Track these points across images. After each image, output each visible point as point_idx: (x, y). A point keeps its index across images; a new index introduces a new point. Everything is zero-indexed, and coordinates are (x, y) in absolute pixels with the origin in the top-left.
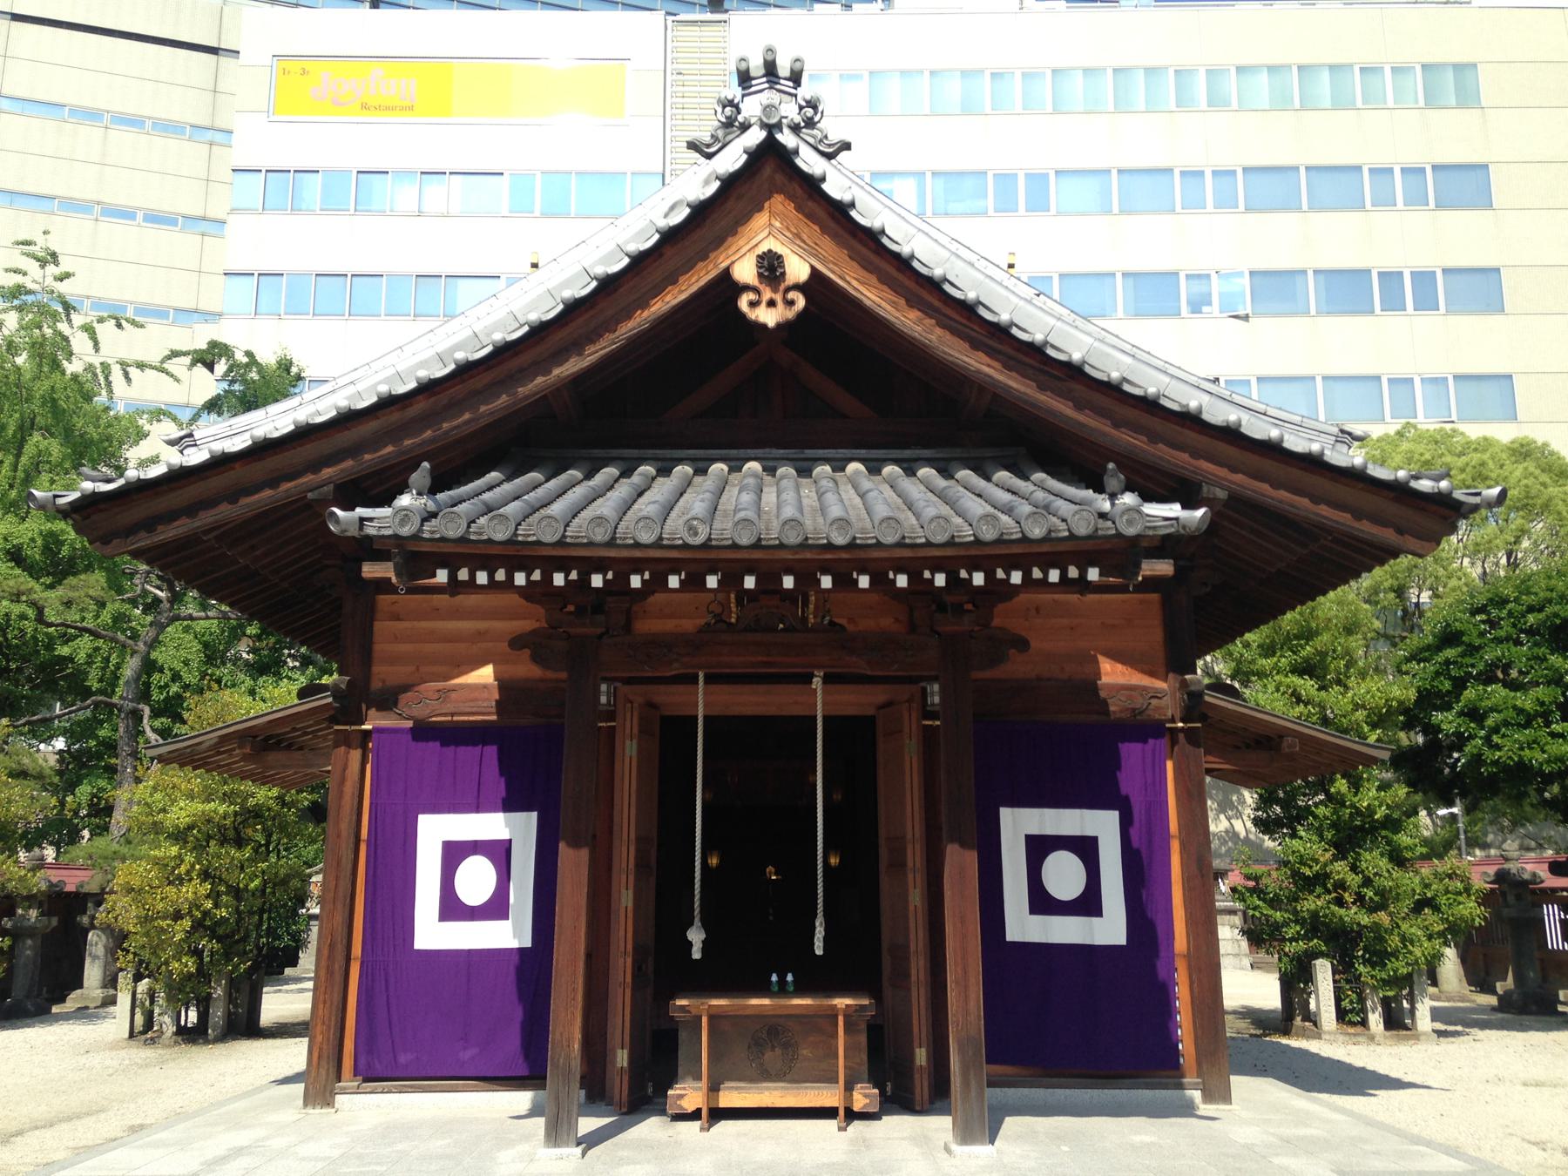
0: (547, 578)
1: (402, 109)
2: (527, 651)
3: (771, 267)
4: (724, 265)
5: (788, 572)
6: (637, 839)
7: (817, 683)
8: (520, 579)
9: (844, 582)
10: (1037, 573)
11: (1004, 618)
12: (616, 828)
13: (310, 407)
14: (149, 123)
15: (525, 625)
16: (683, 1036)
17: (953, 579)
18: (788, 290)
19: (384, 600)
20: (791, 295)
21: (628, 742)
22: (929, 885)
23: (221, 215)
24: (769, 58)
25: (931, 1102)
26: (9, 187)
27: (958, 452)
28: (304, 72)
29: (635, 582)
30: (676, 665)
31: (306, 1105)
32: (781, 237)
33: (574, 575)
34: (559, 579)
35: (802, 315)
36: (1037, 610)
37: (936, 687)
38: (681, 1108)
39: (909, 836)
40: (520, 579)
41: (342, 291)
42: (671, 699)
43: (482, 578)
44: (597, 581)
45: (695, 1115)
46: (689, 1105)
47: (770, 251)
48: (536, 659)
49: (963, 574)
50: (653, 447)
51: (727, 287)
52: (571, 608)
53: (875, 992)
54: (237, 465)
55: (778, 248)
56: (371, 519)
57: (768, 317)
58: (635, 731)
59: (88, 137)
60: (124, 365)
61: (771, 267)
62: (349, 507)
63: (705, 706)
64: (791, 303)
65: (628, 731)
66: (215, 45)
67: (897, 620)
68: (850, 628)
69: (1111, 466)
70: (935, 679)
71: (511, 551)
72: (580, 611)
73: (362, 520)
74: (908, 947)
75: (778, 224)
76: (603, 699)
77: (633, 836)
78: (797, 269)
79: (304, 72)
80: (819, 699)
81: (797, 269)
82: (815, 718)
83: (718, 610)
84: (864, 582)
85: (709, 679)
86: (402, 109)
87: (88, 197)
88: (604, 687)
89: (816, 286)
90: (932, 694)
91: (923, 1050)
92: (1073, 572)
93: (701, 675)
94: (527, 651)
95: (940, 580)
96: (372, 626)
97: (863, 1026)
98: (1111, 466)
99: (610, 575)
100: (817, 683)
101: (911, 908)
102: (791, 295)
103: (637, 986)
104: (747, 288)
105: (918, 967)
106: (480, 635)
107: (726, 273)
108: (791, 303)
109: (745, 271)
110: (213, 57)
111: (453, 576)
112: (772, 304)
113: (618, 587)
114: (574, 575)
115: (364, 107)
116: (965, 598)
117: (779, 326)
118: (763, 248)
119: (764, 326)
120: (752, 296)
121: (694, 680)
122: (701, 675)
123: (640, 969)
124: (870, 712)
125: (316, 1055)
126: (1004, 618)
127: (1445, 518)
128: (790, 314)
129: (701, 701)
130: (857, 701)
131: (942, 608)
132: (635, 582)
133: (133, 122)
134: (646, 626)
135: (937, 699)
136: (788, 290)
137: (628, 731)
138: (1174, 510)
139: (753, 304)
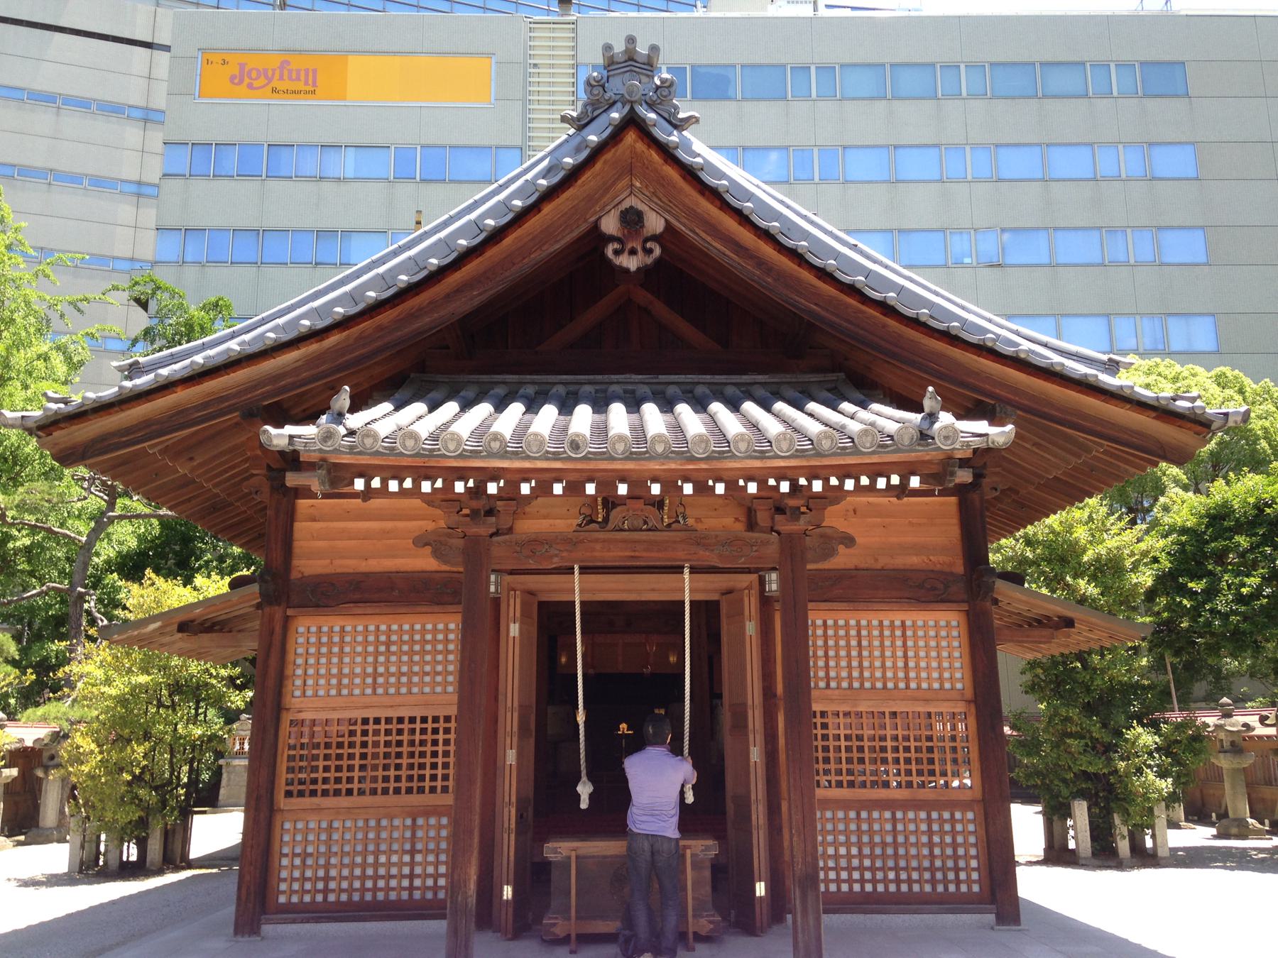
0: (449, 486)
1: (306, 92)
2: (428, 549)
3: (632, 219)
4: (593, 219)
5: (623, 481)
6: (520, 706)
7: (686, 571)
8: (426, 487)
9: (702, 489)
10: (834, 481)
11: (834, 518)
12: (501, 697)
13: (227, 341)
14: (94, 107)
15: (429, 526)
16: (555, 875)
17: (795, 487)
18: (646, 240)
19: (303, 503)
20: (649, 245)
21: (512, 625)
22: (766, 743)
23: (157, 181)
24: (631, 46)
25: (769, 926)
26: (6, 83)
27: (788, 378)
28: (224, 62)
29: (525, 489)
30: (556, 560)
31: (236, 933)
32: (641, 196)
33: (439, 484)
34: (459, 487)
35: (658, 262)
36: (855, 511)
37: (774, 576)
38: (554, 934)
39: (750, 702)
40: (881, 483)
41: (258, 244)
42: (550, 587)
43: (393, 486)
44: (492, 488)
45: (565, 941)
46: (560, 931)
47: (631, 207)
48: (437, 554)
49: (803, 481)
50: (537, 373)
51: (596, 238)
52: (466, 511)
53: (720, 835)
54: (179, 389)
55: (641, 206)
56: (299, 437)
57: (631, 263)
58: (518, 615)
59: (42, 119)
60: (73, 304)
61: (632, 219)
62: (279, 425)
63: (581, 591)
64: (650, 251)
65: (511, 614)
66: (149, 40)
67: (737, 519)
68: (699, 526)
69: (931, 389)
70: (774, 569)
71: (418, 462)
72: (474, 514)
73: (291, 437)
74: (749, 797)
75: (638, 184)
76: (492, 589)
77: (516, 704)
78: (655, 223)
79: (224, 62)
80: (687, 588)
81: (655, 223)
82: (683, 602)
83: (588, 512)
84: (720, 489)
85: (583, 570)
86: (306, 92)
87: (88, 95)
88: (493, 578)
89: (669, 236)
90: (770, 583)
91: (763, 884)
92: (865, 481)
93: (576, 567)
94: (428, 549)
95: (785, 487)
96: (292, 526)
97: (708, 864)
98: (931, 389)
99: (502, 484)
100: (686, 571)
101: (752, 764)
102: (649, 245)
103: (519, 832)
104: (612, 239)
105: (759, 814)
106: (385, 534)
107: (596, 227)
108: (650, 251)
109: (610, 225)
110: (149, 51)
111: (368, 484)
112: (633, 252)
113: (509, 493)
114: (439, 484)
115: (274, 90)
116: (802, 502)
117: (639, 269)
118: (626, 205)
119: (627, 271)
120: (616, 246)
121: (570, 571)
122: (576, 567)
123: (521, 816)
124: (714, 597)
125: (244, 891)
126: (834, 518)
127: (1198, 434)
128: (649, 260)
129: (577, 589)
130: (711, 586)
131: (780, 510)
132: (525, 489)
133: (83, 104)
134: (528, 526)
135: (774, 587)
136: (646, 240)
137: (511, 614)
138: (981, 426)
139: (617, 253)
